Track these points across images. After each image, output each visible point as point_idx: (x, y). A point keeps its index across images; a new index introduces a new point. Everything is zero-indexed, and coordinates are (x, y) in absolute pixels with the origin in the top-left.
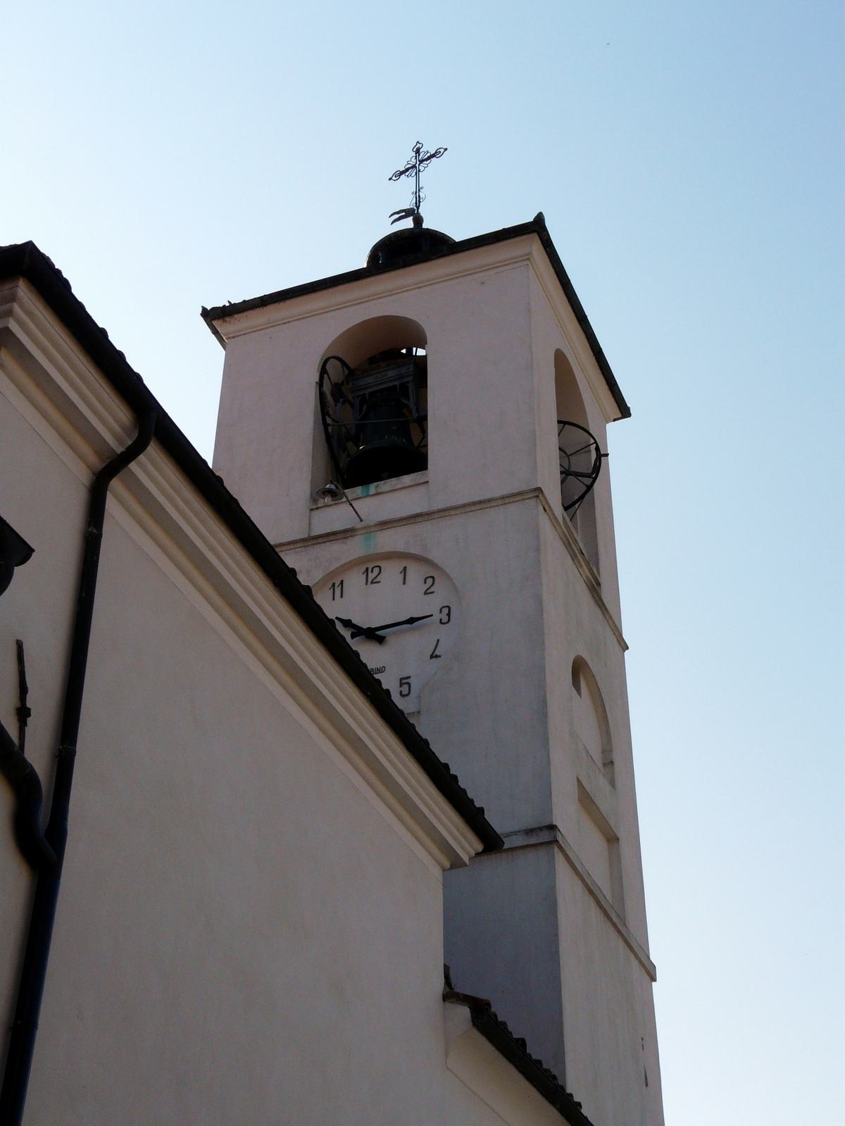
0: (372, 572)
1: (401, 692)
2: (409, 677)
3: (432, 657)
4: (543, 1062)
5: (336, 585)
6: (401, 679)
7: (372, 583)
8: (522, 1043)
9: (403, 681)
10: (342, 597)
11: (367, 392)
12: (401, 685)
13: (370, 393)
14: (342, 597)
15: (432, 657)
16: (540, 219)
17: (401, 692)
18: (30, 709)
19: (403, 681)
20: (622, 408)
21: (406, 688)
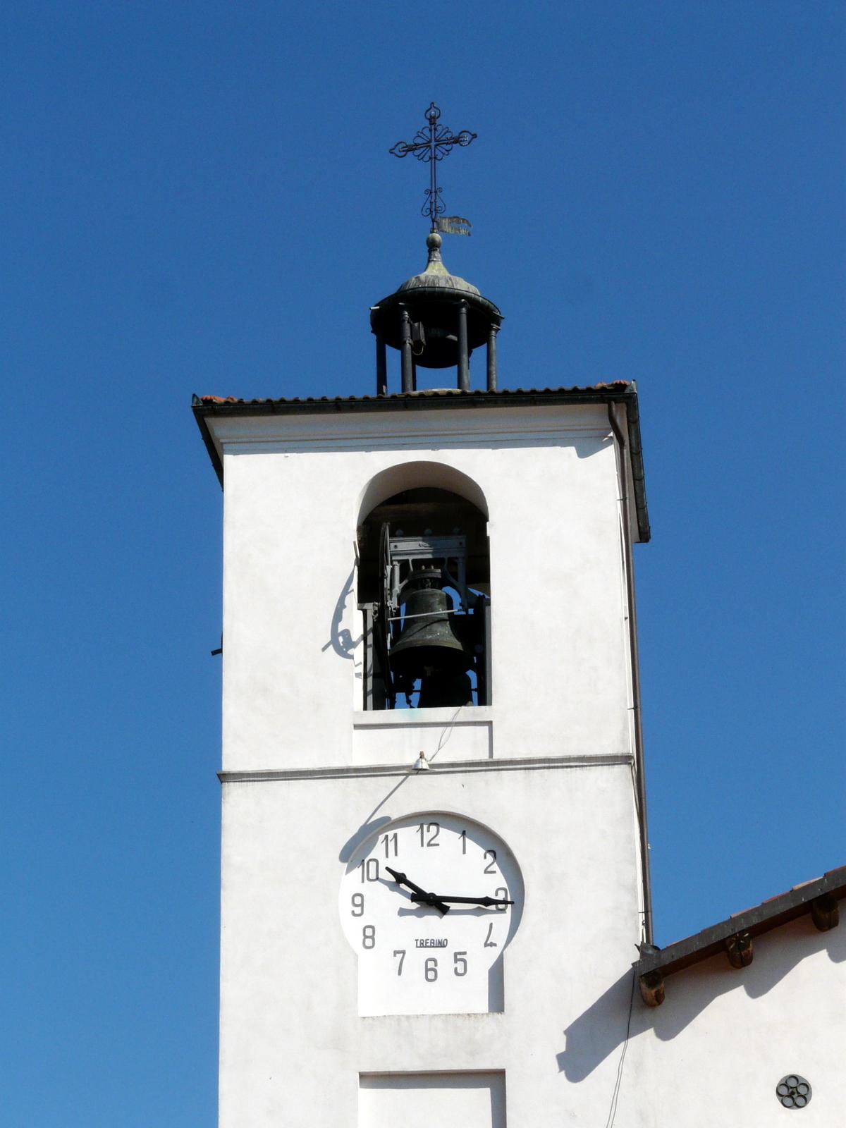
0: (428, 831)
1: (456, 969)
2: (464, 953)
3: (486, 945)
4: (257, 399)
5: (389, 838)
6: (456, 954)
7: (429, 845)
8: (345, 607)
9: (459, 957)
10: (396, 854)
11: (410, 558)
12: (456, 960)
13: (414, 561)
14: (396, 854)
15: (486, 945)
16: (485, 946)
17: (456, 969)
18: (566, 1032)
19: (459, 957)
20: (459, 1022)
21: (460, 966)
